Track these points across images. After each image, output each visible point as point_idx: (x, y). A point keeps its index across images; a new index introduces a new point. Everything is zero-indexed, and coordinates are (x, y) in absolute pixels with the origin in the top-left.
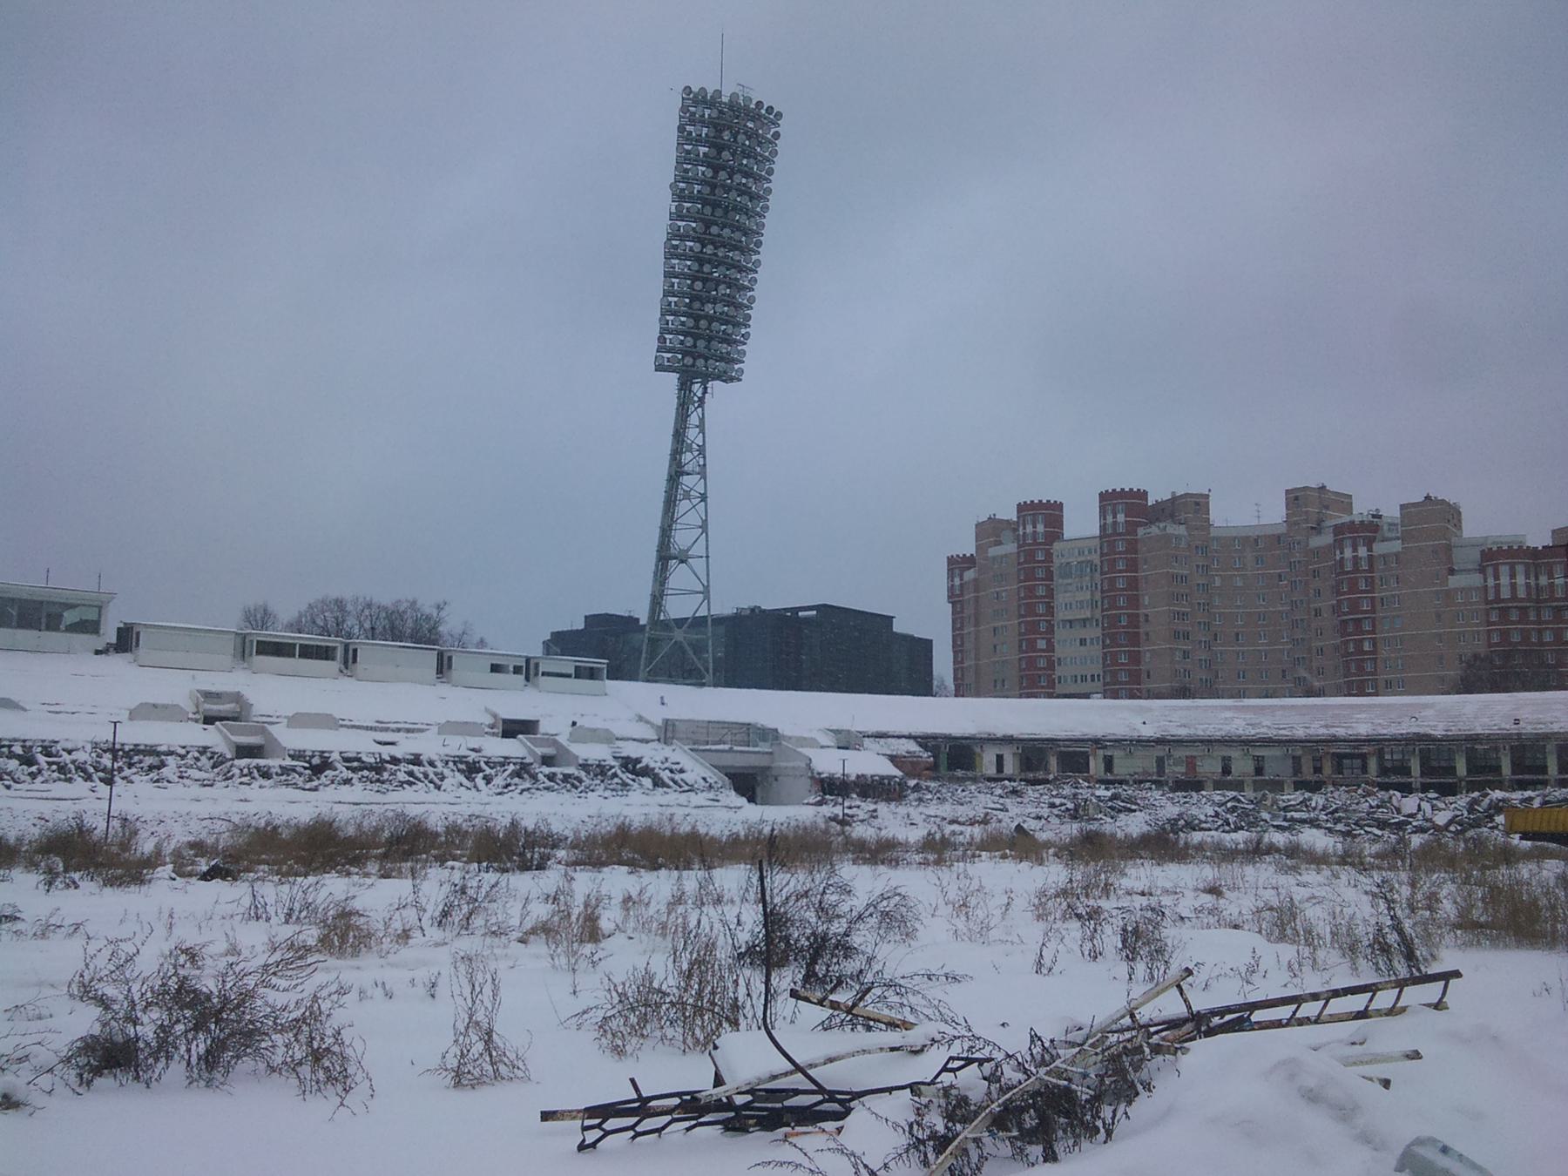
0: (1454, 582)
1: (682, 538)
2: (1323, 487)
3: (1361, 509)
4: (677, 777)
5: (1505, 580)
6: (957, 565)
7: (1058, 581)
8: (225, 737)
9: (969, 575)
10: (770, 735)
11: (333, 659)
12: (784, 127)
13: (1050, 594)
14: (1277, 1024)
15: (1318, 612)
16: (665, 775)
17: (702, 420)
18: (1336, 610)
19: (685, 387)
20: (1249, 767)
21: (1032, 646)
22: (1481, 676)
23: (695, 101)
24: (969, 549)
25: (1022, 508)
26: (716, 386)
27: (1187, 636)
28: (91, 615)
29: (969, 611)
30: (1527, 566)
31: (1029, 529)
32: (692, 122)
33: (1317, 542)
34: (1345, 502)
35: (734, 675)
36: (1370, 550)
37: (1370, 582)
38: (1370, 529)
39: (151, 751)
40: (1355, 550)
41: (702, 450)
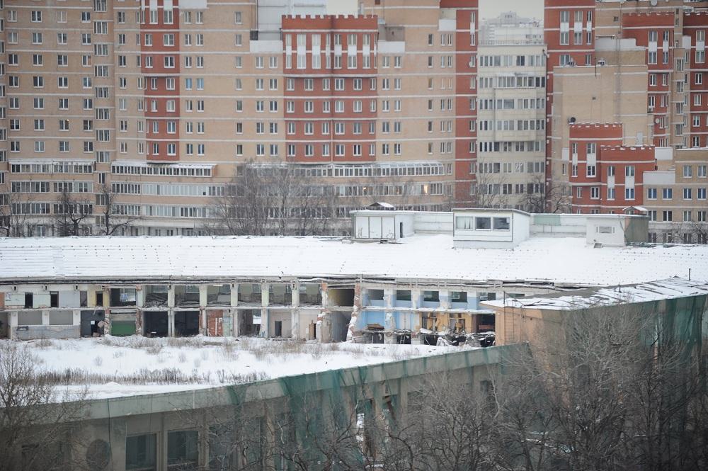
0: (256, 47)
5: (301, 50)
14: (521, 287)
15: (122, 60)
20: (47, 300)
30: (323, 36)
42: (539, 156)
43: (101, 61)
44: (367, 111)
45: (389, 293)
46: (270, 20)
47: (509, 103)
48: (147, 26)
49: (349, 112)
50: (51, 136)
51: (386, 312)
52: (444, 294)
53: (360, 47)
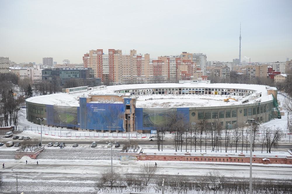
0: (150, 63)
5: (155, 64)
42: (176, 75)
43: (132, 65)
44: (161, 70)
45: (185, 89)
46: (151, 61)
47: (173, 69)
50: (126, 73)
51: (185, 91)
52: (192, 89)
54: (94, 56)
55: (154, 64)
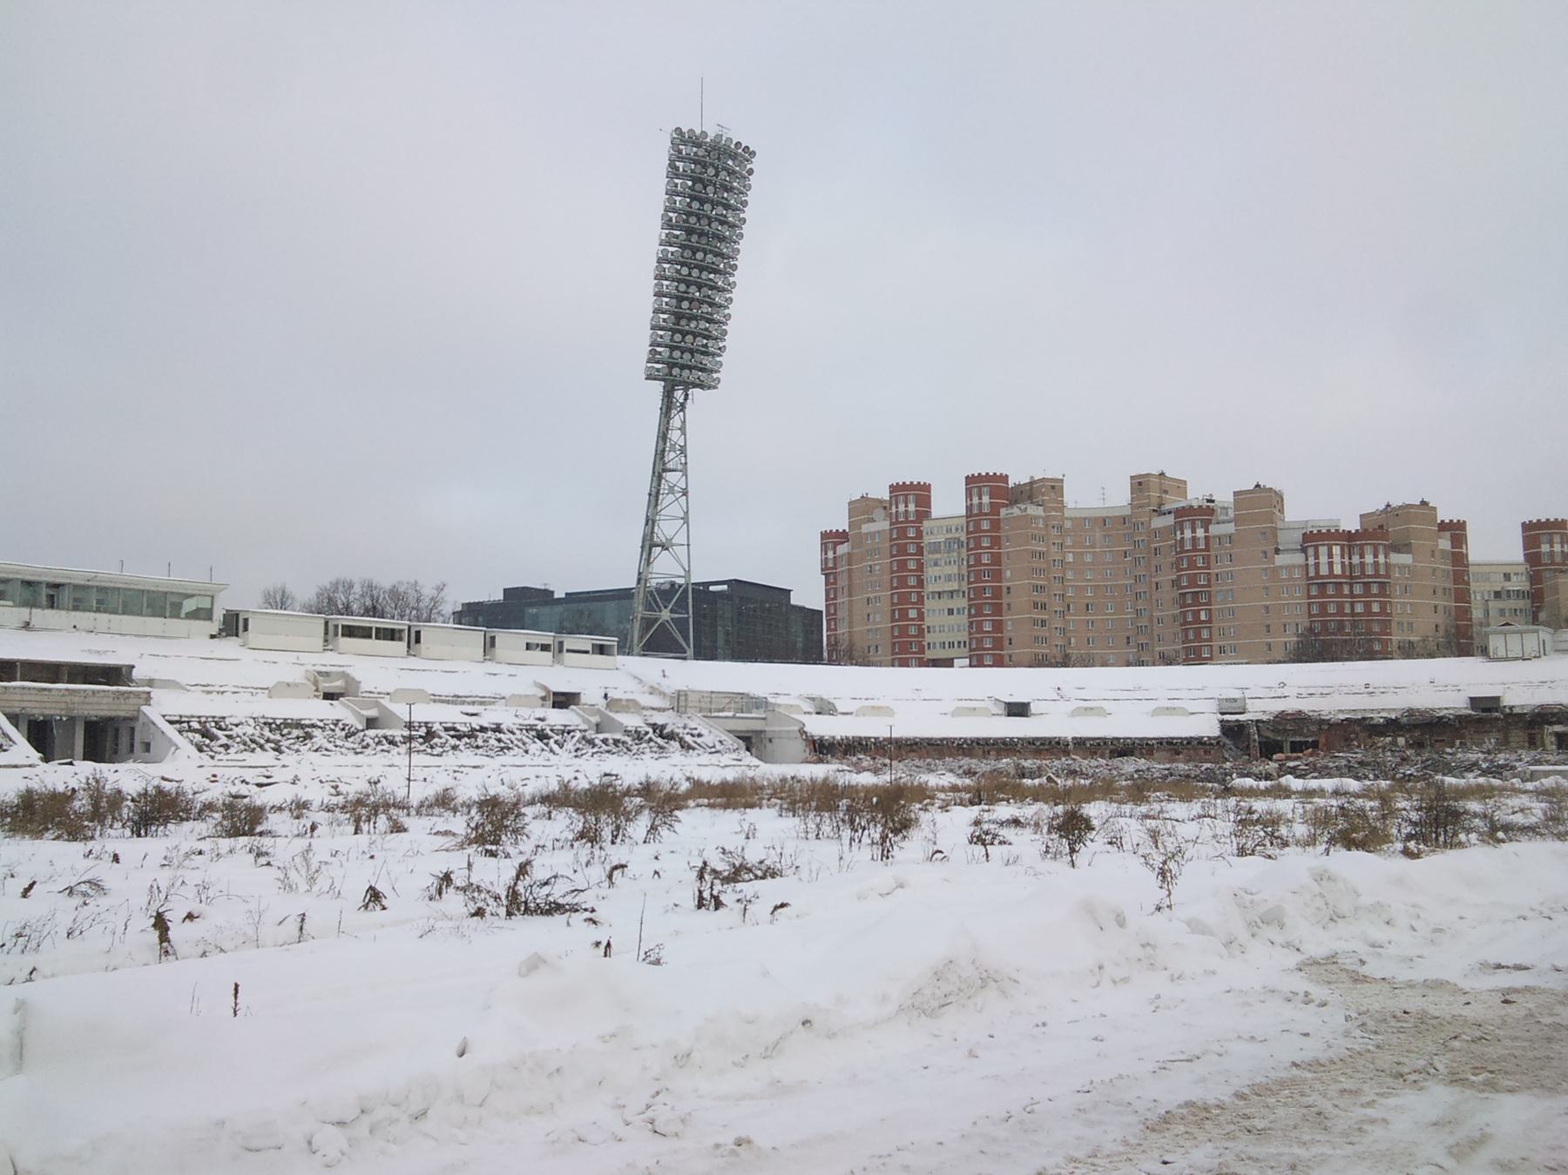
0: (1280, 560)
1: (665, 529)
2: (1162, 474)
3: (1195, 495)
4: (699, 740)
5: (1323, 559)
6: (831, 539)
7: (928, 557)
8: (354, 711)
9: (843, 549)
10: (759, 703)
11: (400, 639)
12: (755, 164)
13: (920, 567)
16: (688, 739)
17: (684, 422)
18: (1176, 583)
19: (668, 395)
21: (904, 615)
22: (1316, 647)
23: (683, 139)
24: (843, 525)
25: (894, 489)
26: (695, 392)
27: (1044, 606)
28: (206, 604)
29: (842, 582)
31: (902, 508)
32: (681, 159)
33: (1159, 522)
34: (1181, 486)
35: (659, 643)
36: (1207, 531)
37: (1207, 559)
38: (1205, 513)
39: (298, 725)
40: (1194, 531)
41: (683, 450)
46: (1293, 538)
48: (1186, 623)
49: (1368, 611)
53: (1376, 556)
54: (872, 535)
55: (1311, 561)
